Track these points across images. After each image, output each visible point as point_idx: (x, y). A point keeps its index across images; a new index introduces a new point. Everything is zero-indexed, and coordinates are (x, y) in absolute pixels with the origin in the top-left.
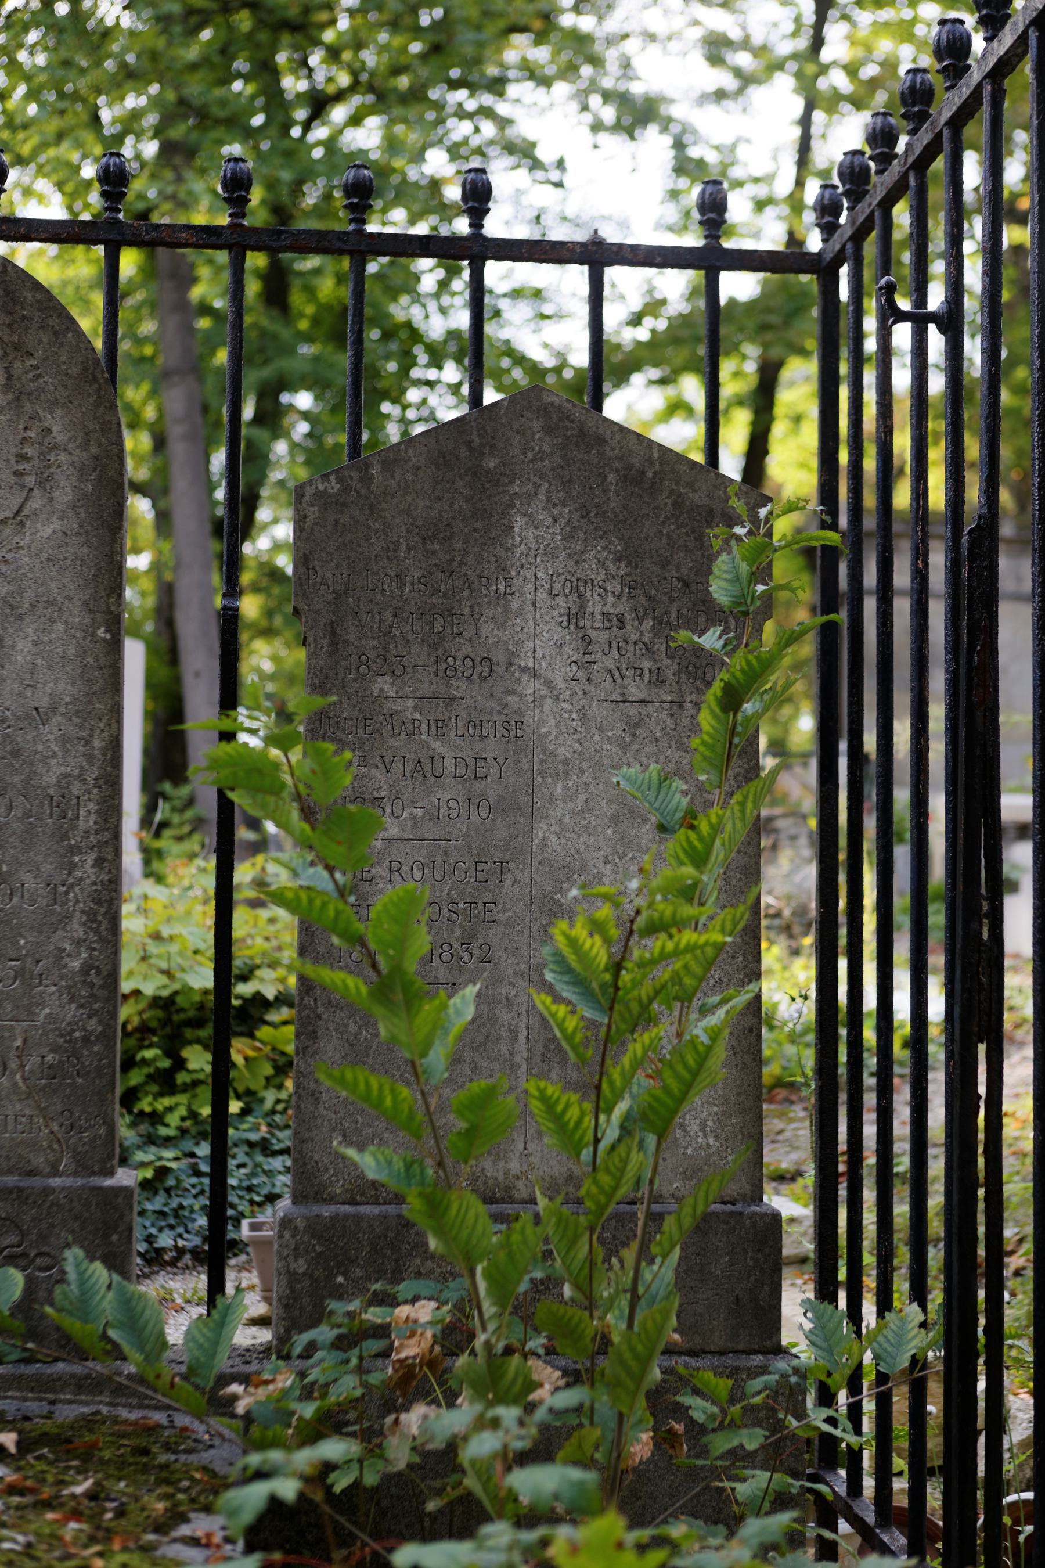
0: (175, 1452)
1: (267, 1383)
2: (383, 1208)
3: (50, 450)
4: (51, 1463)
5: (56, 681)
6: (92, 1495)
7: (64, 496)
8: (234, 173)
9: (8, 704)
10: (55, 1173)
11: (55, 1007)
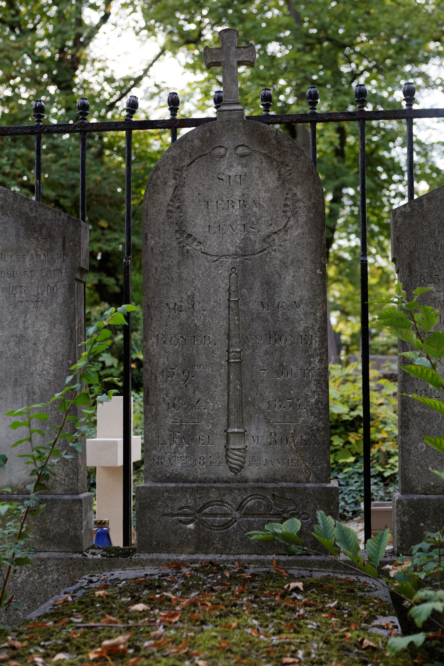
0: (363, 592)
1: (400, 565)
2: (438, 496)
3: (296, 202)
4: (317, 595)
5: (302, 291)
6: (338, 607)
7: (302, 219)
8: (360, 90)
9: (284, 300)
10: (308, 482)
11: (306, 417)
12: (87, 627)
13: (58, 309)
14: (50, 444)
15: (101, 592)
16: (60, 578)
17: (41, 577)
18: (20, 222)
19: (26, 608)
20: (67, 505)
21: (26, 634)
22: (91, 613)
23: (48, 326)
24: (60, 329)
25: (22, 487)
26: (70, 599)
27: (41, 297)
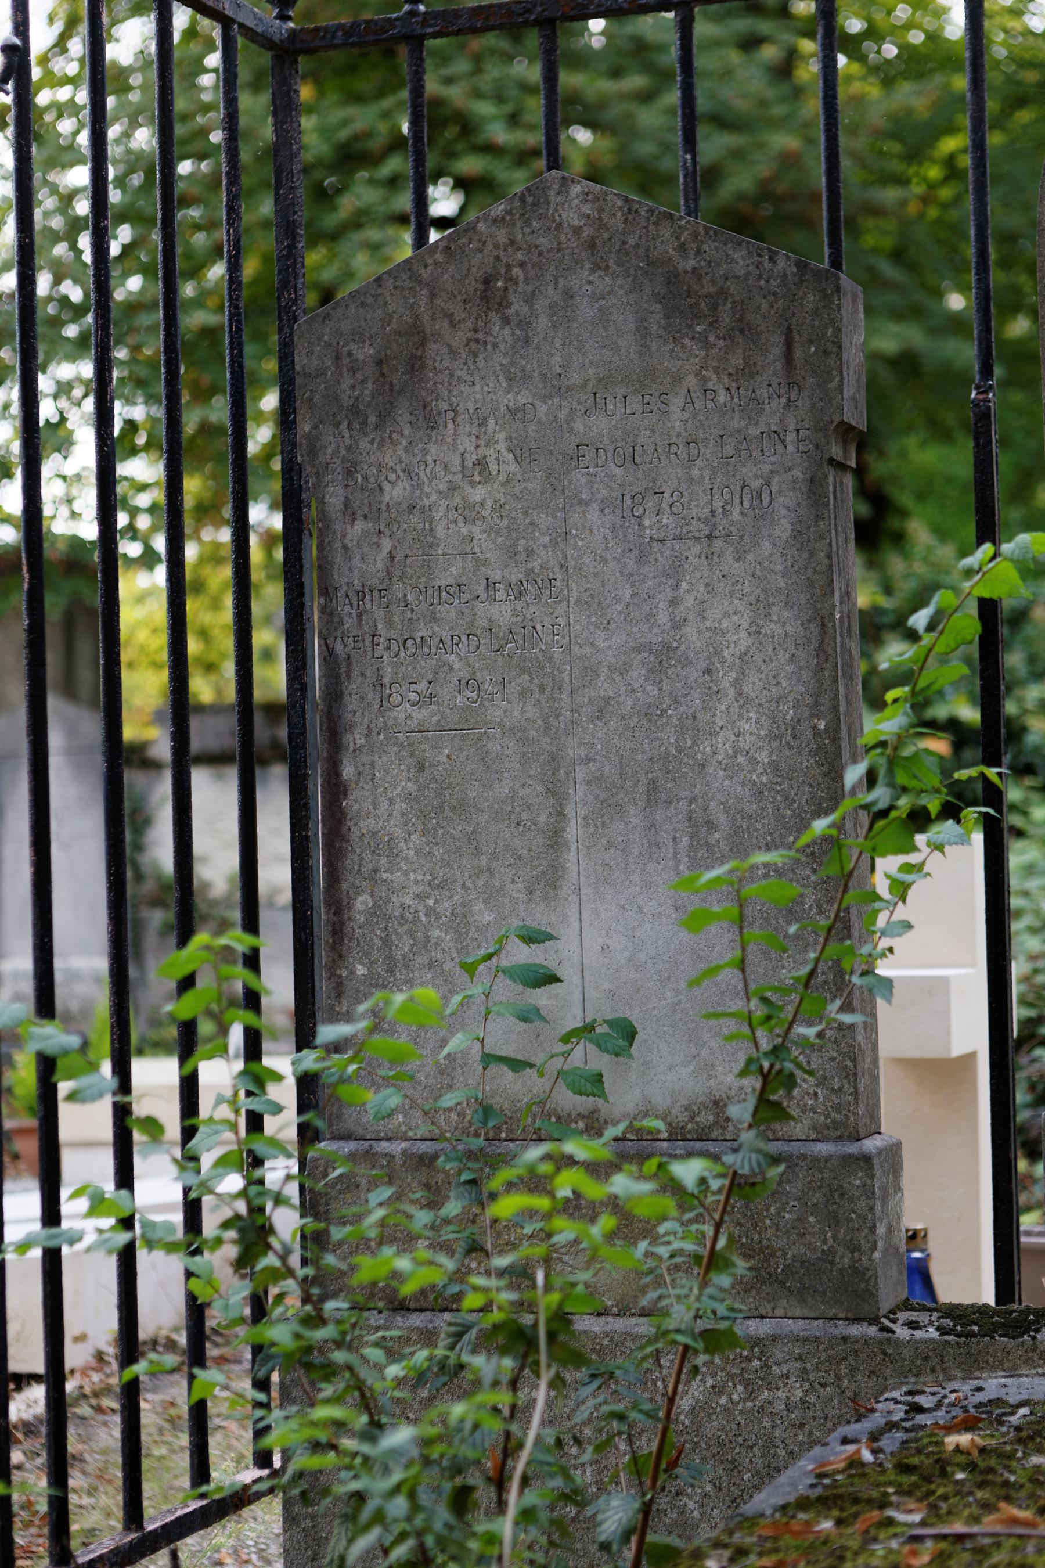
12: (944, 1537)
13: (777, 557)
14: (797, 980)
15: (964, 1439)
16: (812, 1399)
17: (751, 1395)
18: (647, 291)
19: (708, 1488)
20: (827, 1174)
21: (761, 1554)
22: (945, 1498)
23: (747, 614)
24: (786, 623)
25: (683, 1118)
26: (867, 1456)
27: (722, 523)
